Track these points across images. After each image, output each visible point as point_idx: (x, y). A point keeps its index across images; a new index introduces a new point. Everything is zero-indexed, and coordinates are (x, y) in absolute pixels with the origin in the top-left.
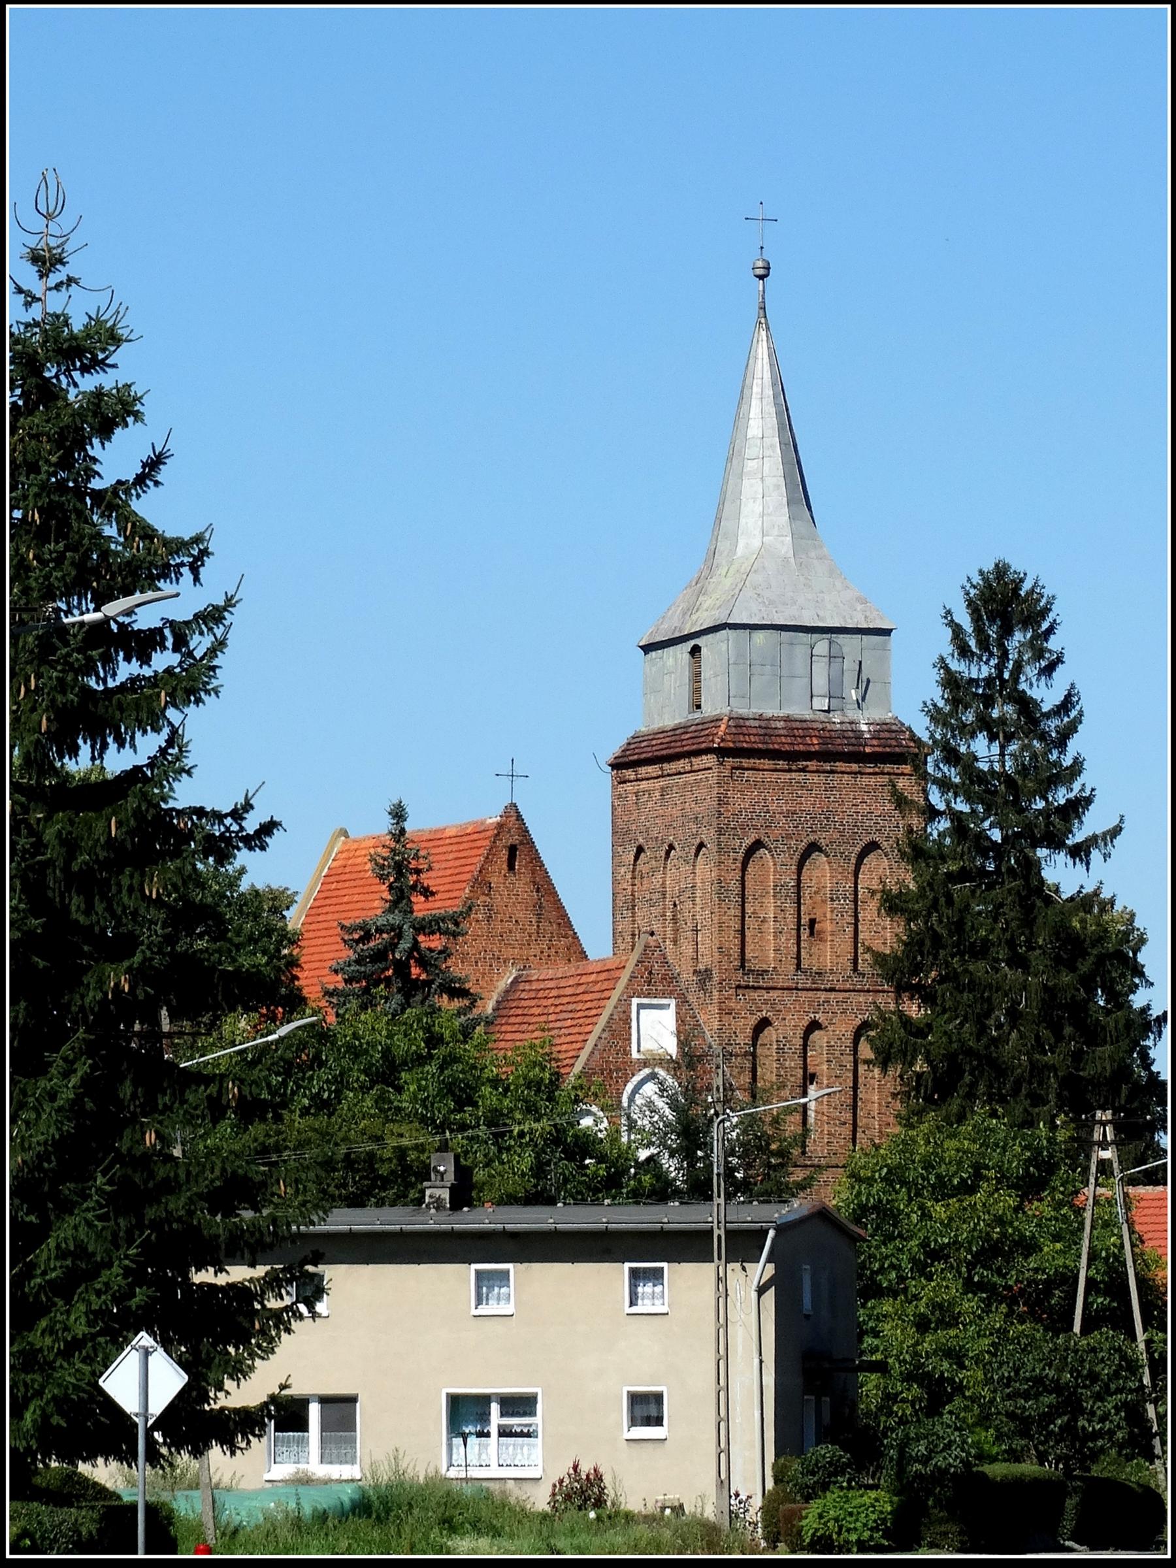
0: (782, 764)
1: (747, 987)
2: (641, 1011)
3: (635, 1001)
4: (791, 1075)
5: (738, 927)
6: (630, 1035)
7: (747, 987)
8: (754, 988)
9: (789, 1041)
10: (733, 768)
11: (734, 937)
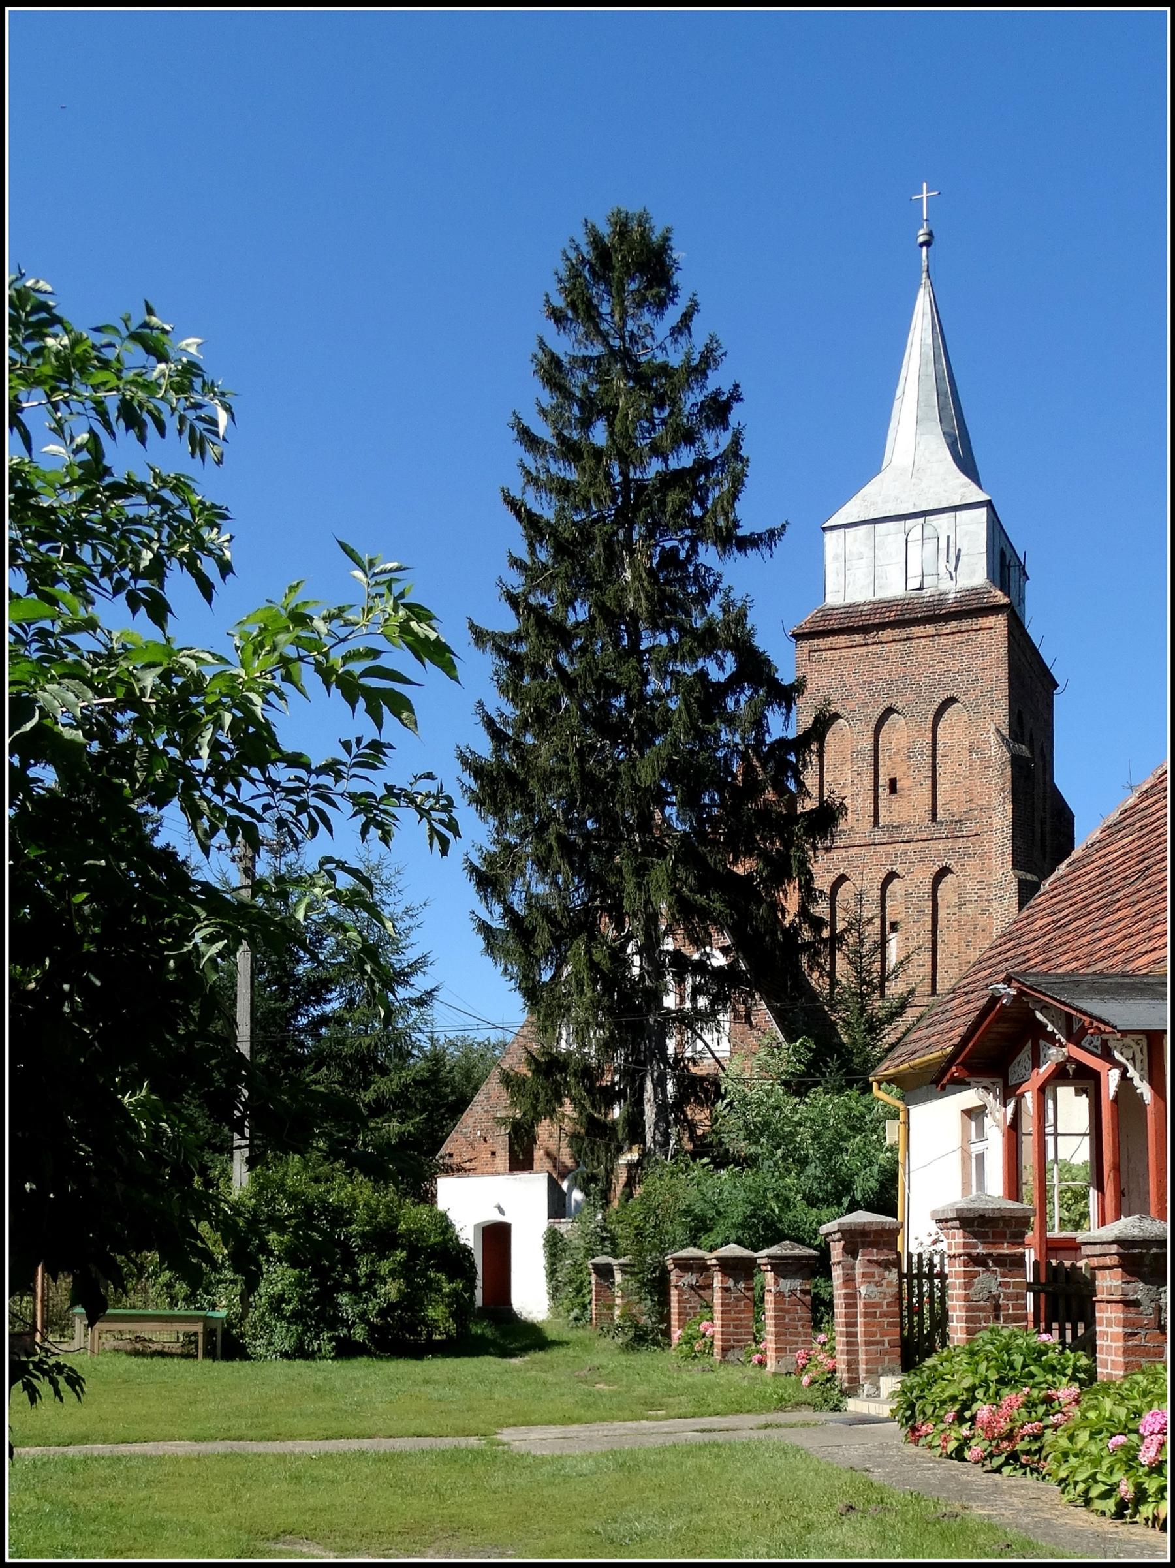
0: (858, 638)
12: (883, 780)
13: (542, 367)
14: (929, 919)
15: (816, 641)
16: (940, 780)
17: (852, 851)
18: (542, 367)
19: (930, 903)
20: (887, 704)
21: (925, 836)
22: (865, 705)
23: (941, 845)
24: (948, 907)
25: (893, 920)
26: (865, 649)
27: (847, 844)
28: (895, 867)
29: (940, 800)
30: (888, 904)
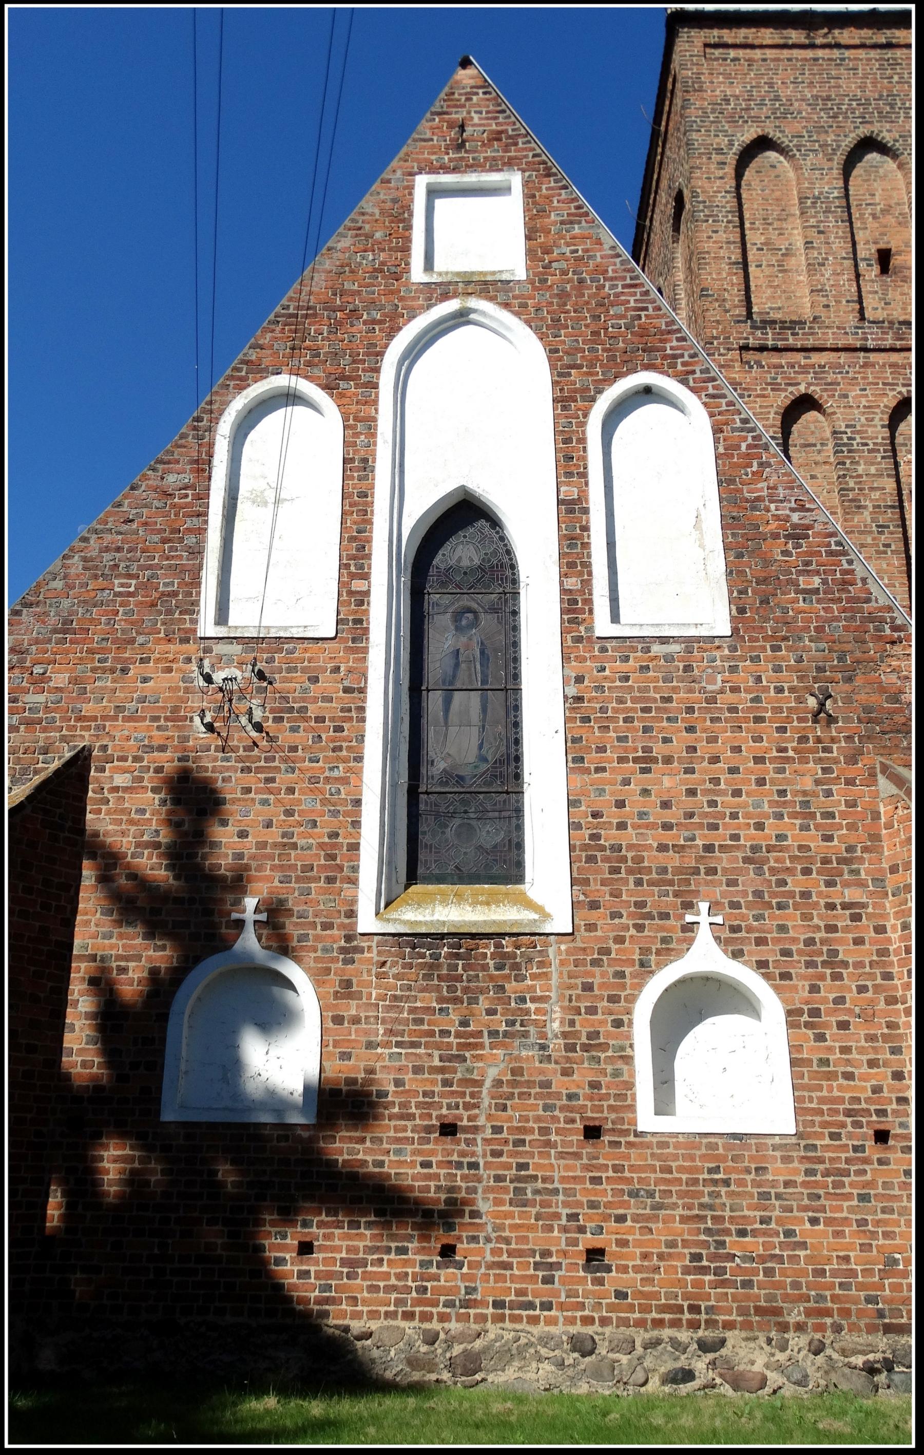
0: (795, 35)
1: (762, 349)
2: (439, 203)
3: (422, 182)
4: (872, 489)
5: (736, 256)
6: (408, 240)
7: (762, 349)
8: (776, 349)
9: (858, 432)
10: (706, 45)
11: (729, 274)
12: (866, 251)
13: (236, 1421)
15: (716, 32)
17: (816, 358)
18: (236, 1421)
20: (864, 131)
22: (821, 130)
26: (809, 54)
27: (810, 342)
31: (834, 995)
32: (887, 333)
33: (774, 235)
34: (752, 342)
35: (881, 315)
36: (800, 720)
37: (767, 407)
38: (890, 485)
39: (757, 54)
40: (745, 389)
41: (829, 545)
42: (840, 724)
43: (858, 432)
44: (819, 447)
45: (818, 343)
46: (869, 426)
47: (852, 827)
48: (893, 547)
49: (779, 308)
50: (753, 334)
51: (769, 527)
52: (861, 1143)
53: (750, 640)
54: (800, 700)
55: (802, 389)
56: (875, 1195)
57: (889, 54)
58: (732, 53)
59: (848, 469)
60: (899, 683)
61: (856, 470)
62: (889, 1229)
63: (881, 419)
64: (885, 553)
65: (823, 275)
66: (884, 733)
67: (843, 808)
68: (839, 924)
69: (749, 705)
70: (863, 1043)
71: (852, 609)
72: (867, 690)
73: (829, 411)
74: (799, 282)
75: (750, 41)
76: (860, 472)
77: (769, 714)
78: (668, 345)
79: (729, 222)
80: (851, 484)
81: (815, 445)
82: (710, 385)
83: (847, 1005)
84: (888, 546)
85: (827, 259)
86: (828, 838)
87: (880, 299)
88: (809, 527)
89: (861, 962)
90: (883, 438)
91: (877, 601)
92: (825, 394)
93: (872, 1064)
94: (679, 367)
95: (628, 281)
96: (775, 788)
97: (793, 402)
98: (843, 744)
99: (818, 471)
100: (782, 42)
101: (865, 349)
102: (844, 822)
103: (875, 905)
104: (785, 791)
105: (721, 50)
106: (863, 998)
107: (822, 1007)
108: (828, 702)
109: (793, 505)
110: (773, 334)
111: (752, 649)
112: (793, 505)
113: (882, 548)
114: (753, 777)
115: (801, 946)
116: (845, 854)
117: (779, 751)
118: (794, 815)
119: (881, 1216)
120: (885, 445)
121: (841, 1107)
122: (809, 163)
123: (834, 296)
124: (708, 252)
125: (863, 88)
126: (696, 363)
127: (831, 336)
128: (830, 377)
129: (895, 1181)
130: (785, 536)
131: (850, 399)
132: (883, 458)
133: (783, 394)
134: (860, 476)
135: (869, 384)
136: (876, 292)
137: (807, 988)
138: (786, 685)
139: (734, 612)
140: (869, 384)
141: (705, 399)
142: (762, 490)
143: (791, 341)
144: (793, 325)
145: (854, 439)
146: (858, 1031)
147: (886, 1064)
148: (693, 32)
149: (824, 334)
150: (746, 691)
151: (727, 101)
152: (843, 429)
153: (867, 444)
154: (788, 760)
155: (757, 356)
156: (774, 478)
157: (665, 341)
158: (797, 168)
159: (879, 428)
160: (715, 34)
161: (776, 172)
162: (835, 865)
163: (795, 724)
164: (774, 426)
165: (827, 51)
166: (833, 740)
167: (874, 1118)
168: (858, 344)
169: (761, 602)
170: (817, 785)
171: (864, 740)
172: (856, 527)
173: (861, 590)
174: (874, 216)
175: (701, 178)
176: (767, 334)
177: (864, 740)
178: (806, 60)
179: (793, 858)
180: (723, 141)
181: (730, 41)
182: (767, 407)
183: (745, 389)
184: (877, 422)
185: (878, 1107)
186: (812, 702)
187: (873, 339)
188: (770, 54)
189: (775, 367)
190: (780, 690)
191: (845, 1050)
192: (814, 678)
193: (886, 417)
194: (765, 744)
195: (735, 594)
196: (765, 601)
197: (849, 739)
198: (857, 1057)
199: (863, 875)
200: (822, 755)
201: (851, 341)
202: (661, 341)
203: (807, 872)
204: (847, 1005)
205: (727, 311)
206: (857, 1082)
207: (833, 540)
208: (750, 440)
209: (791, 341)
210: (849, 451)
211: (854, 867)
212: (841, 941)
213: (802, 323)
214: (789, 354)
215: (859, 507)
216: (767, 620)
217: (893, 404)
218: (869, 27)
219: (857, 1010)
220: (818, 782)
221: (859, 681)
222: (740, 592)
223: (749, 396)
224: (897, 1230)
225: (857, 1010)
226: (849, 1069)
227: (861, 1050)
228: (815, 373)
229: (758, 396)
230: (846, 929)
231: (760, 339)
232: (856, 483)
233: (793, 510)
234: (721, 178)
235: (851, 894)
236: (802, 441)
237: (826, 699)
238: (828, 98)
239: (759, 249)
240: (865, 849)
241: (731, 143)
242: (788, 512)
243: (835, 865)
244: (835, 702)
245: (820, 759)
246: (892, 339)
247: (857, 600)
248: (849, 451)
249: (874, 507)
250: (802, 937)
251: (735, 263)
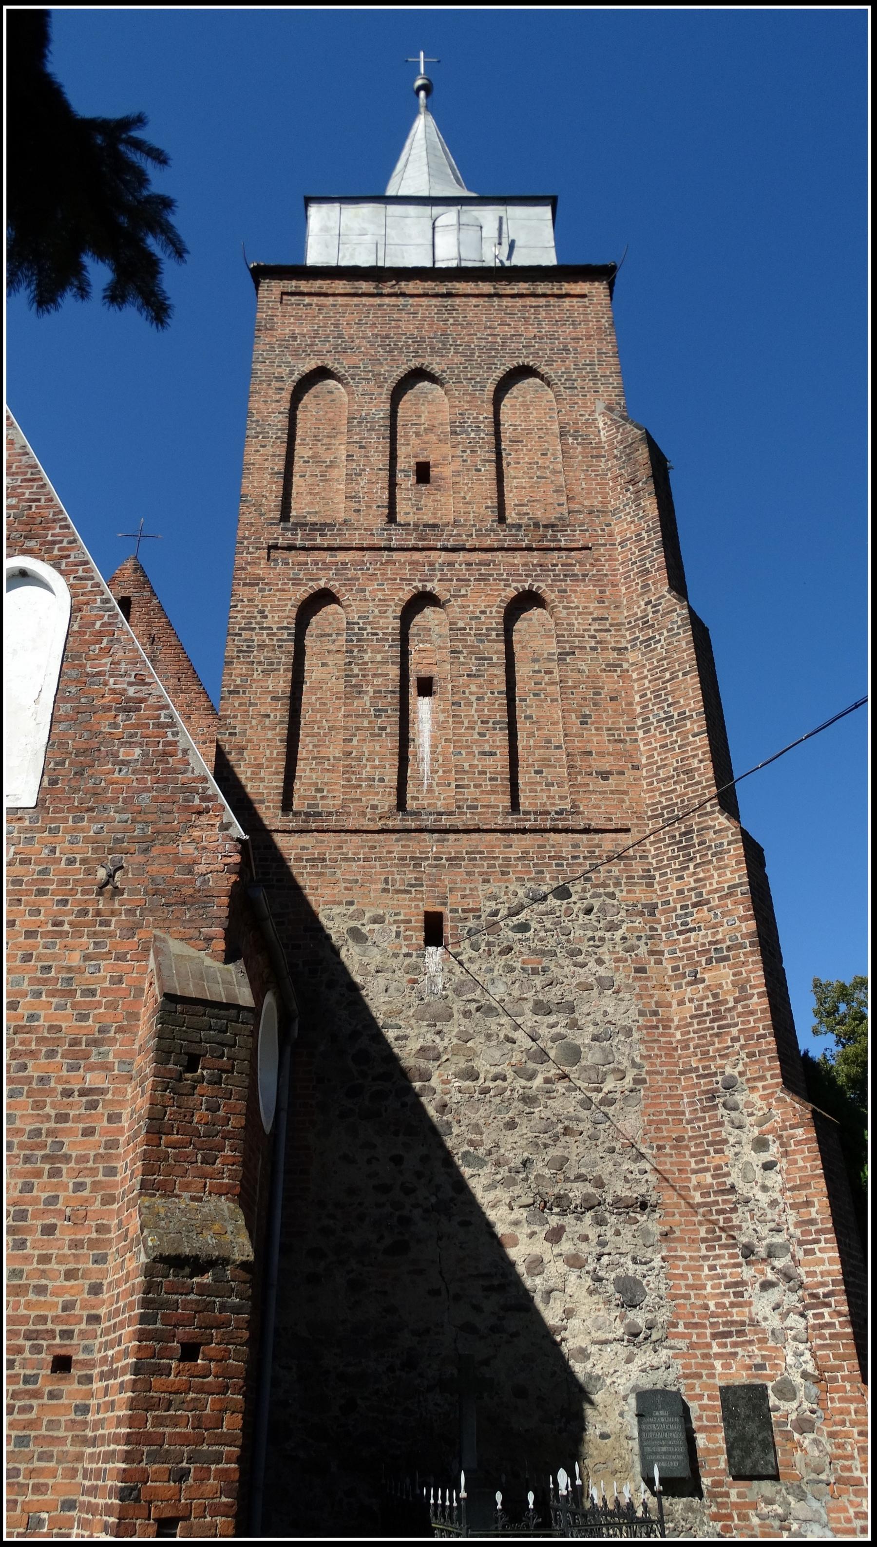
0: (365, 286)
5: (280, 466)
7: (291, 548)
8: (304, 549)
9: (370, 623)
12: (405, 463)
14: (501, 671)
15: (294, 283)
16: (509, 472)
17: (341, 556)
19: (502, 647)
20: (415, 363)
21: (488, 542)
22: (376, 361)
23: (518, 558)
24: (535, 661)
25: (424, 673)
26: (377, 301)
27: (338, 542)
28: (429, 586)
29: (511, 498)
30: (414, 646)
31: (47, 1195)
32: (411, 535)
33: (321, 449)
34: (281, 542)
35: (412, 519)
36: (84, 892)
37: (284, 600)
38: (394, 671)
39: (331, 300)
40: (267, 584)
41: (159, 717)
42: (125, 896)
43: (370, 623)
44: (334, 637)
45: (343, 543)
46: (381, 617)
47: (112, 1006)
48: (388, 730)
49: (316, 513)
50: (283, 534)
51: (104, 700)
52: (35, 1372)
53: (54, 812)
54: (88, 872)
55: (322, 584)
56: (36, 1437)
57: (449, 301)
58: (307, 300)
59: (354, 657)
60: (196, 853)
61: (362, 658)
62: (41, 1481)
63: (394, 611)
64: (380, 735)
65: (358, 484)
66: (168, 905)
67: (107, 985)
68: (72, 1113)
69: (35, 877)
70: (66, 1251)
71: (165, 780)
72: (161, 861)
73: (347, 603)
74: (338, 490)
75: (324, 290)
76: (366, 659)
77: (54, 886)
78: (50, 533)
79: (277, 438)
80: (356, 671)
81: (330, 635)
82: (81, 568)
83: (58, 1206)
84: (384, 729)
85: (364, 470)
86: (83, 1017)
87: (413, 505)
88: (142, 700)
89: (85, 1155)
90: (393, 629)
91: (193, 772)
92: (343, 589)
93: (70, 1275)
94: (56, 552)
95: (29, 476)
96: (40, 964)
97: (311, 595)
98: (123, 917)
99: (330, 660)
100: (353, 291)
101: (390, 549)
102: (105, 1000)
103: (116, 1091)
104: (50, 967)
105: (297, 298)
106: (77, 1197)
107: (30, 1209)
108: (118, 874)
109: (132, 679)
110: (303, 535)
111: (53, 820)
112: (132, 679)
113: (377, 731)
114: (20, 953)
115: (25, 1138)
116: (97, 1035)
117: (55, 924)
118: (52, 994)
119: (37, 1464)
120: (395, 634)
121: (23, 1328)
122: (360, 389)
123: (366, 502)
124: (253, 464)
125: (419, 328)
126: (73, 548)
127: (357, 537)
128: (351, 574)
129: (63, 1419)
130: (117, 709)
131: (367, 593)
132: (390, 646)
133: (303, 589)
134: (366, 663)
135: (387, 579)
136: (410, 499)
137: (19, 1186)
138: (78, 857)
139: (45, 784)
140: (387, 579)
141: (72, 581)
142: (105, 665)
143: (319, 541)
144: (321, 528)
145: (365, 629)
146: (64, 1235)
147: (86, 1274)
148: (274, 283)
149: (351, 535)
150: (36, 864)
151: (294, 338)
152: (355, 620)
153: (377, 634)
154: (63, 935)
155: (285, 554)
156: (120, 654)
157: (49, 528)
158: (350, 393)
159: (391, 619)
160: (292, 285)
161: (333, 397)
162: (84, 1047)
163: (79, 896)
164: (288, 617)
165: (393, 299)
166: (113, 913)
167: (58, 1341)
168: (383, 544)
169: (76, 773)
170: (85, 961)
171: (146, 912)
172: (354, 711)
173: (180, 761)
174: (417, 434)
175: (257, 401)
176: (297, 535)
177: (146, 912)
178: (372, 305)
179: (40, 1040)
180: (284, 371)
181: (306, 290)
182: (284, 600)
183: (267, 584)
184: (390, 614)
185: (65, 1327)
186: (102, 874)
187: (397, 540)
188: (341, 300)
189: (299, 564)
190: (71, 862)
191: (45, 1259)
192: (109, 849)
193: (399, 609)
194: (42, 917)
195: (52, 765)
196: (79, 773)
197: (130, 912)
198: (56, 1267)
199: (111, 1058)
200: (98, 928)
201: (376, 541)
202: (44, 529)
203: (51, 1054)
204: (58, 1206)
205: (261, 515)
206: (49, 1298)
207: (163, 713)
208: (106, 619)
209: (318, 541)
210: (359, 640)
211: (103, 1049)
212: (69, 1132)
213: (331, 526)
214: (316, 552)
215: (360, 692)
216: (76, 790)
217: (407, 597)
218: (433, 280)
219: (68, 1211)
220: (86, 958)
221: (154, 852)
222: (57, 764)
223: (270, 590)
224: (51, 1481)
225: (68, 1211)
226: (43, 1282)
227: (62, 1259)
228: (336, 569)
229: (278, 590)
230: (78, 1118)
231: (289, 539)
232: (360, 670)
233: (131, 684)
234: (277, 401)
235: (93, 1079)
236: (319, 632)
237: (116, 871)
238: (387, 337)
239: (305, 462)
240: (120, 1030)
241: (291, 373)
242: (125, 686)
243: (84, 1047)
244: (126, 873)
245: (95, 933)
246: (415, 539)
247: (175, 771)
248: (359, 640)
249: (375, 692)
250: (28, 1128)
251: (276, 473)
